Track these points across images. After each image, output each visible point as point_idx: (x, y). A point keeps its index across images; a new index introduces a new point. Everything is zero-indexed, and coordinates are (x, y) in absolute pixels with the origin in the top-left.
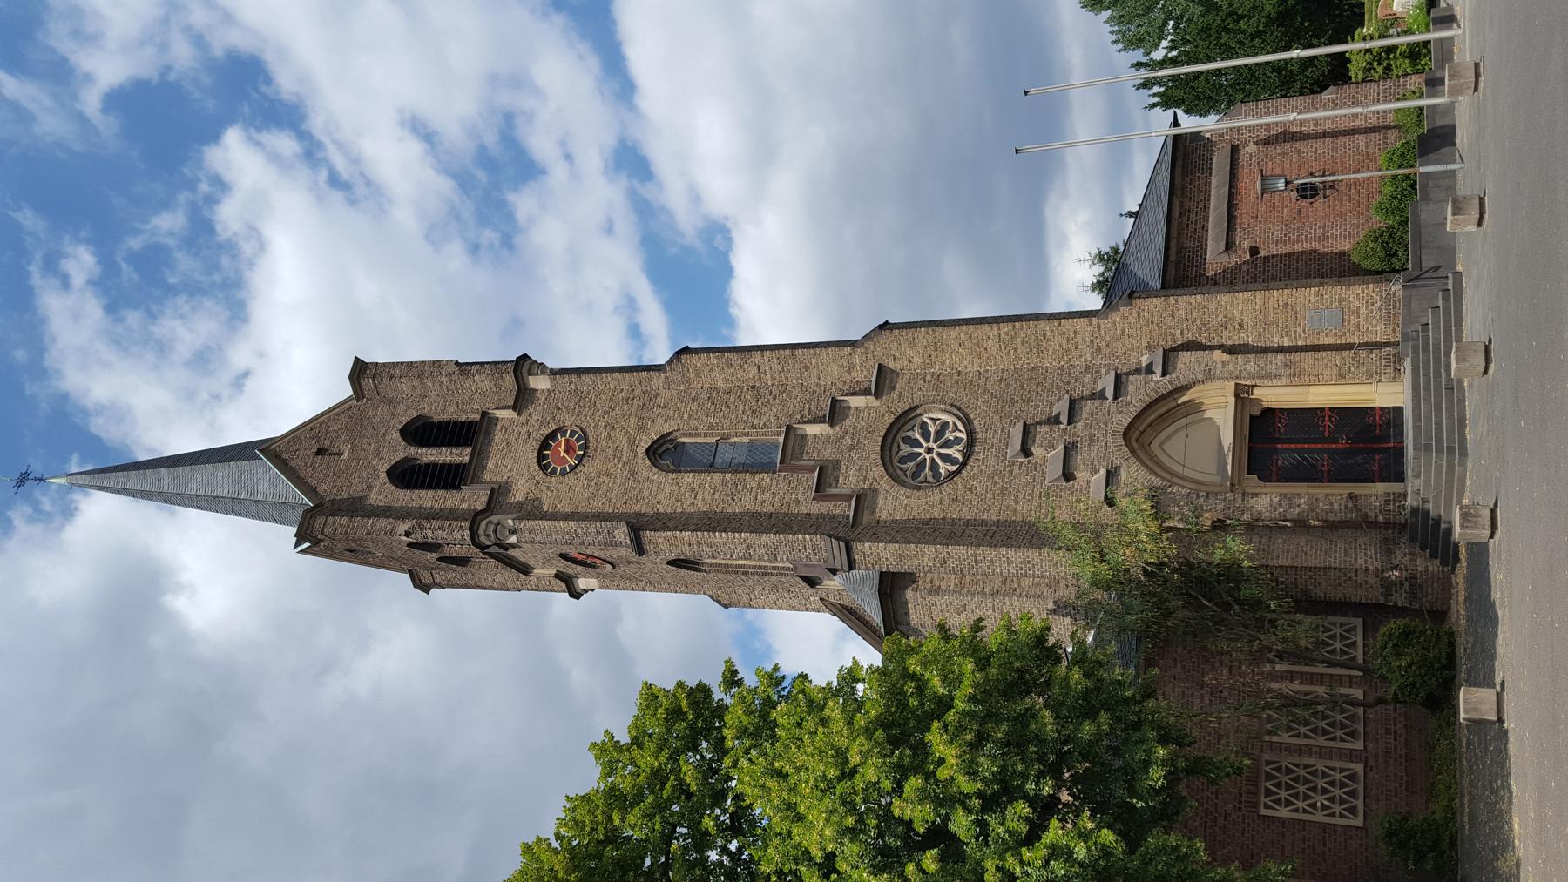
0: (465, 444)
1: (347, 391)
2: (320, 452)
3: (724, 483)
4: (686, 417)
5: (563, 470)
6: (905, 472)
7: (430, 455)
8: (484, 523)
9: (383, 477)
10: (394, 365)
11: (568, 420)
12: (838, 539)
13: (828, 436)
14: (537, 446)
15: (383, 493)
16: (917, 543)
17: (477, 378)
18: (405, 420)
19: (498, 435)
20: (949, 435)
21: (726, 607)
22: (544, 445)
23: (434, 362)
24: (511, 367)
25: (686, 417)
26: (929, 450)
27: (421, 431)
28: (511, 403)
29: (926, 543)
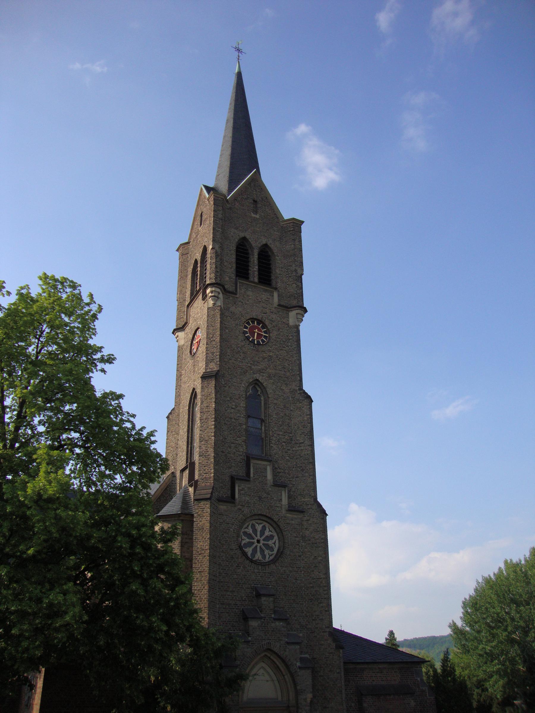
0: (259, 278)
1: (286, 216)
2: (255, 202)
3: (241, 425)
4: (275, 401)
5: (246, 332)
6: (247, 528)
7: (254, 259)
8: (219, 290)
9: (242, 235)
10: (300, 241)
11: (274, 334)
12: (212, 494)
13: (266, 484)
14: (260, 317)
15: (235, 235)
16: (210, 538)
17: (294, 285)
18: (272, 246)
19: (264, 296)
20: (266, 552)
21: (168, 417)
22: (259, 322)
23: (302, 263)
24: (300, 304)
25: (275, 401)
26: (258, 541)
27: (265, 255)
28: (282, 303)
29: (210, 544)
